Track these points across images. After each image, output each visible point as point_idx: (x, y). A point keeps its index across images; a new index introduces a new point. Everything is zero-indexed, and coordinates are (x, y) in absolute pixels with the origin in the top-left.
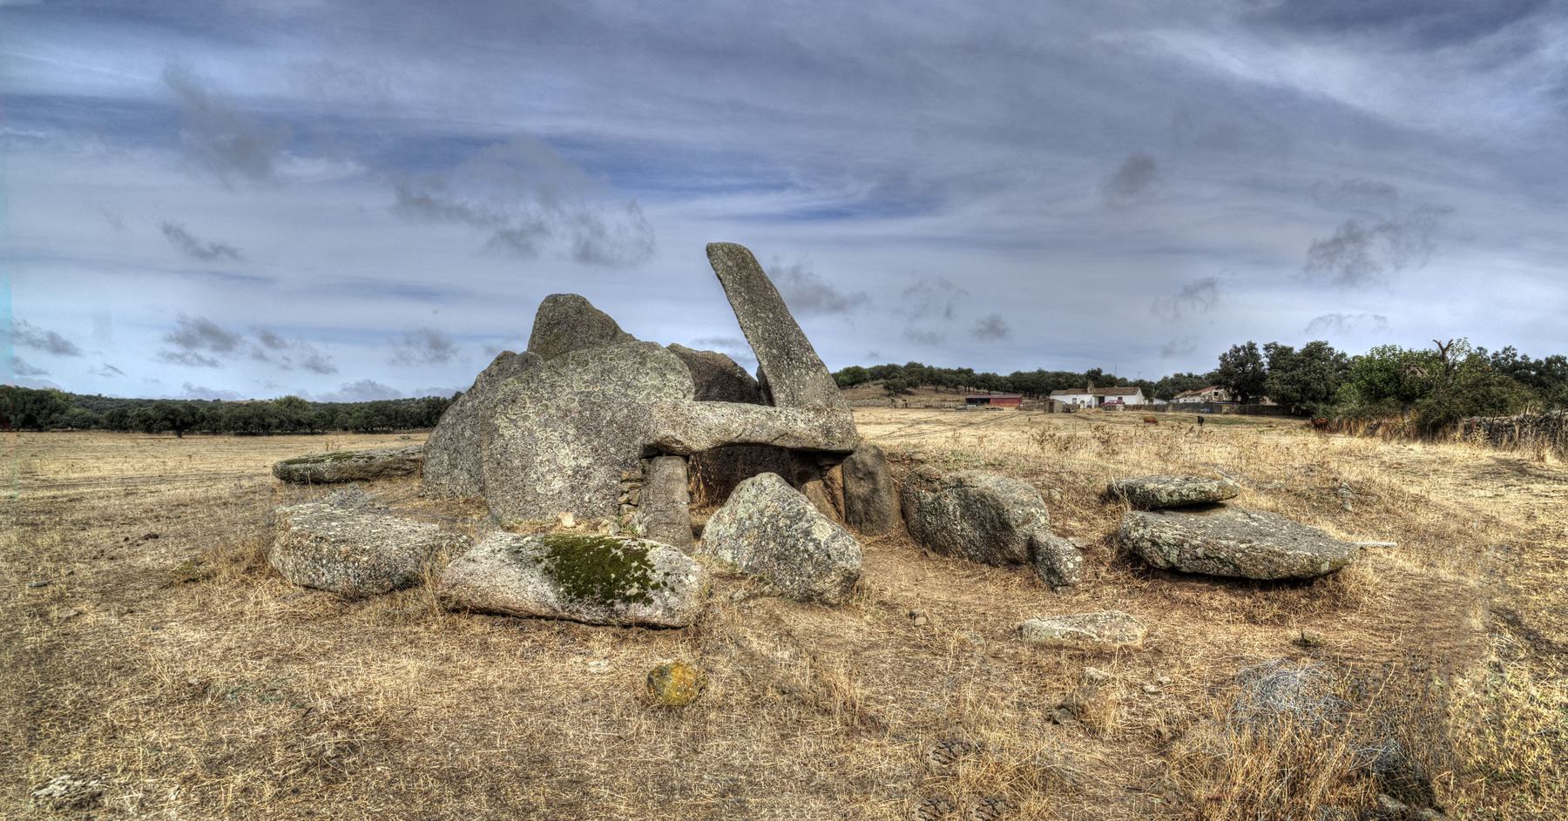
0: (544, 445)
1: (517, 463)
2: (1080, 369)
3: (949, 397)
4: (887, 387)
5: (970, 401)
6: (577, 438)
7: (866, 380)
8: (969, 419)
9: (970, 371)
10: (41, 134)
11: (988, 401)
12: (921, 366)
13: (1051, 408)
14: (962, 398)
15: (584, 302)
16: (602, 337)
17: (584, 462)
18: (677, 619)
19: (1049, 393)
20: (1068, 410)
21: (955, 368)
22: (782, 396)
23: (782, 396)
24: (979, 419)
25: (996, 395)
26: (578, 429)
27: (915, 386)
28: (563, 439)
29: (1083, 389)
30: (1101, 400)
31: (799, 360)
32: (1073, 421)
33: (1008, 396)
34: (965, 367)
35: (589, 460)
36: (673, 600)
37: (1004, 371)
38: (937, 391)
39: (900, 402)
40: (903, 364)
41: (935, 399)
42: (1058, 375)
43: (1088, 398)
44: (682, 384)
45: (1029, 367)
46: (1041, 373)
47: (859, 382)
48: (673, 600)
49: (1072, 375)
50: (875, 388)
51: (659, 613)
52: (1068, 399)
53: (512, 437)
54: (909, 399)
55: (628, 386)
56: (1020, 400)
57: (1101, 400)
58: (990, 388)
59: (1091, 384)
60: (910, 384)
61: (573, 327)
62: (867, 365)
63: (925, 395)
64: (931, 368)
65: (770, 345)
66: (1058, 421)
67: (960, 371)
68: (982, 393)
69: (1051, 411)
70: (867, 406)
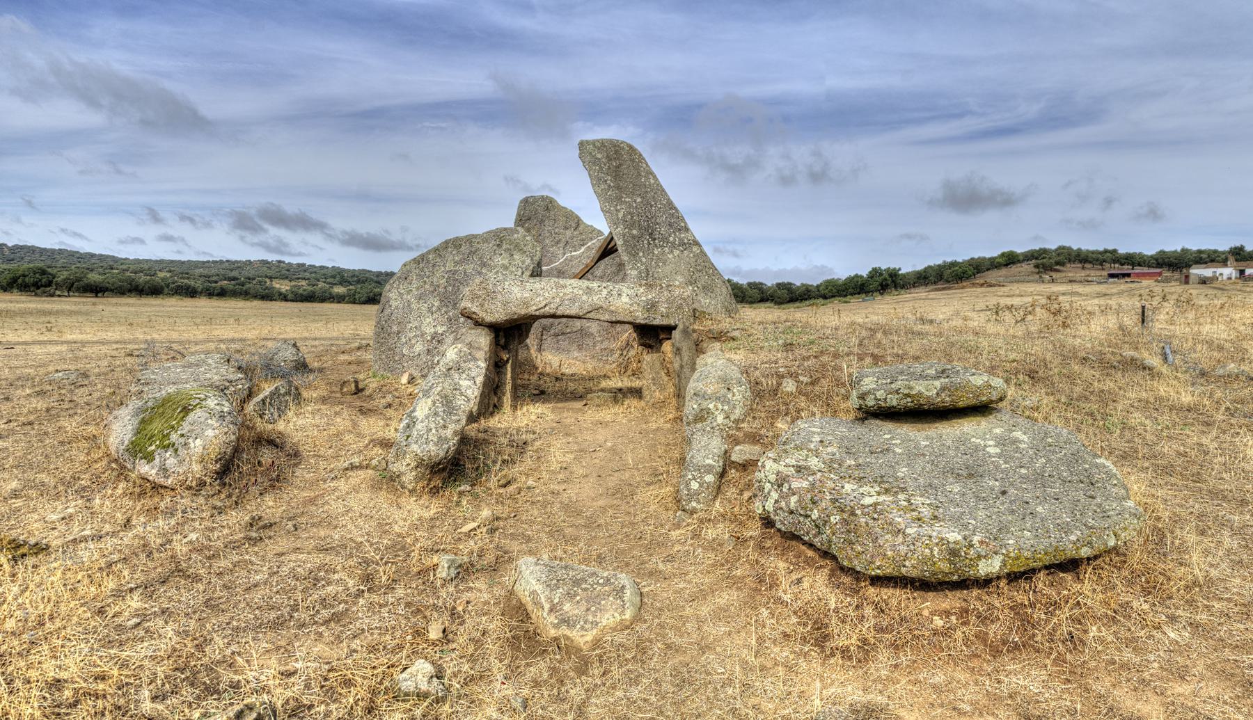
0: (415, 314)
1: (395, 328)
2: (1223, 246)
3: (1093, 273)
4: (1037, 266)
5: (1112, 276)
6: (439, 309)
7: (1019, 261)
8: (1104, 291)
9: (1115, 251)
10: (444, 125)
11: (1129, 275)
12: (1070, 248)
13: (1187, 280)
14: (1105, 273)
15: (552, 201)
16: (566, 228)
17: (440, 330)
18: (170, 481)
19: (1189, 266)
20: (1204, 281)
21: (1101, 249)
22: (634, 273)
23: (634, 273)
24: (1114, 291)
25: (1138, 270)
26: (441, 301)
27: (1063, 264)
28: (430, 310)
29: (1224, 263)
30: (1242, 272)
31: (665, 239)
32: (1211, 292)
33: (1152, 270)
34: (1110, 248)
35: (444, 328)
36: (171, 462)
37: (1150, 251)
38: (1083, 268)
39: (1047, 277)
40: (1053, 247)
41: (1081, 274)
42: (1200, 252)
43: (1228, 272)
44: (523, 262)
45: (1173, 245)
46: (1184, 251)
47: (1014, 263)
48: (171, 462)
49: (1215, 251)
50: (1027, 267)
51: (154, 472)
52: (1207, 272)
53: (397, 308)
54: (1055, 275)
55: (484, 265)
56: (1160, 274)
57: (1242, 272)
58: (1133, 265)
59: (1231, 259)
60: (1058, 263)
61: (542, 222)
62: (1020, 249)
63: (1073, 271)
64: (1079, 249)
65: (631, 226)
66: (1194, 290)
67: (1106, 251)
68: (1126, 269)
69: (1187, 282)
70: (1018, 282)
